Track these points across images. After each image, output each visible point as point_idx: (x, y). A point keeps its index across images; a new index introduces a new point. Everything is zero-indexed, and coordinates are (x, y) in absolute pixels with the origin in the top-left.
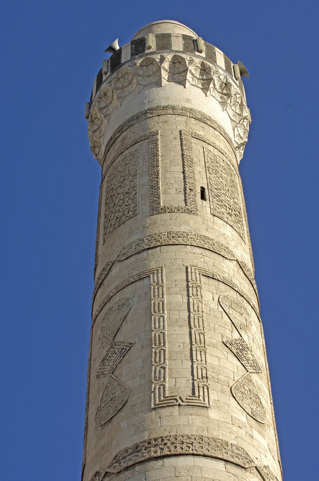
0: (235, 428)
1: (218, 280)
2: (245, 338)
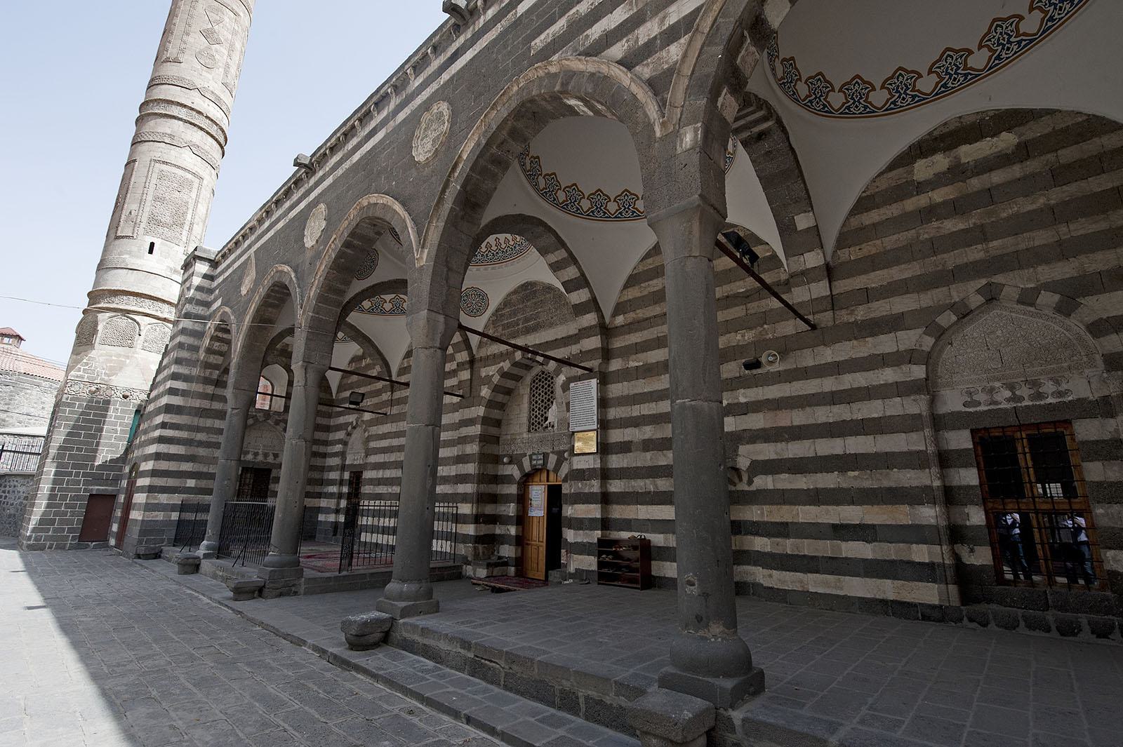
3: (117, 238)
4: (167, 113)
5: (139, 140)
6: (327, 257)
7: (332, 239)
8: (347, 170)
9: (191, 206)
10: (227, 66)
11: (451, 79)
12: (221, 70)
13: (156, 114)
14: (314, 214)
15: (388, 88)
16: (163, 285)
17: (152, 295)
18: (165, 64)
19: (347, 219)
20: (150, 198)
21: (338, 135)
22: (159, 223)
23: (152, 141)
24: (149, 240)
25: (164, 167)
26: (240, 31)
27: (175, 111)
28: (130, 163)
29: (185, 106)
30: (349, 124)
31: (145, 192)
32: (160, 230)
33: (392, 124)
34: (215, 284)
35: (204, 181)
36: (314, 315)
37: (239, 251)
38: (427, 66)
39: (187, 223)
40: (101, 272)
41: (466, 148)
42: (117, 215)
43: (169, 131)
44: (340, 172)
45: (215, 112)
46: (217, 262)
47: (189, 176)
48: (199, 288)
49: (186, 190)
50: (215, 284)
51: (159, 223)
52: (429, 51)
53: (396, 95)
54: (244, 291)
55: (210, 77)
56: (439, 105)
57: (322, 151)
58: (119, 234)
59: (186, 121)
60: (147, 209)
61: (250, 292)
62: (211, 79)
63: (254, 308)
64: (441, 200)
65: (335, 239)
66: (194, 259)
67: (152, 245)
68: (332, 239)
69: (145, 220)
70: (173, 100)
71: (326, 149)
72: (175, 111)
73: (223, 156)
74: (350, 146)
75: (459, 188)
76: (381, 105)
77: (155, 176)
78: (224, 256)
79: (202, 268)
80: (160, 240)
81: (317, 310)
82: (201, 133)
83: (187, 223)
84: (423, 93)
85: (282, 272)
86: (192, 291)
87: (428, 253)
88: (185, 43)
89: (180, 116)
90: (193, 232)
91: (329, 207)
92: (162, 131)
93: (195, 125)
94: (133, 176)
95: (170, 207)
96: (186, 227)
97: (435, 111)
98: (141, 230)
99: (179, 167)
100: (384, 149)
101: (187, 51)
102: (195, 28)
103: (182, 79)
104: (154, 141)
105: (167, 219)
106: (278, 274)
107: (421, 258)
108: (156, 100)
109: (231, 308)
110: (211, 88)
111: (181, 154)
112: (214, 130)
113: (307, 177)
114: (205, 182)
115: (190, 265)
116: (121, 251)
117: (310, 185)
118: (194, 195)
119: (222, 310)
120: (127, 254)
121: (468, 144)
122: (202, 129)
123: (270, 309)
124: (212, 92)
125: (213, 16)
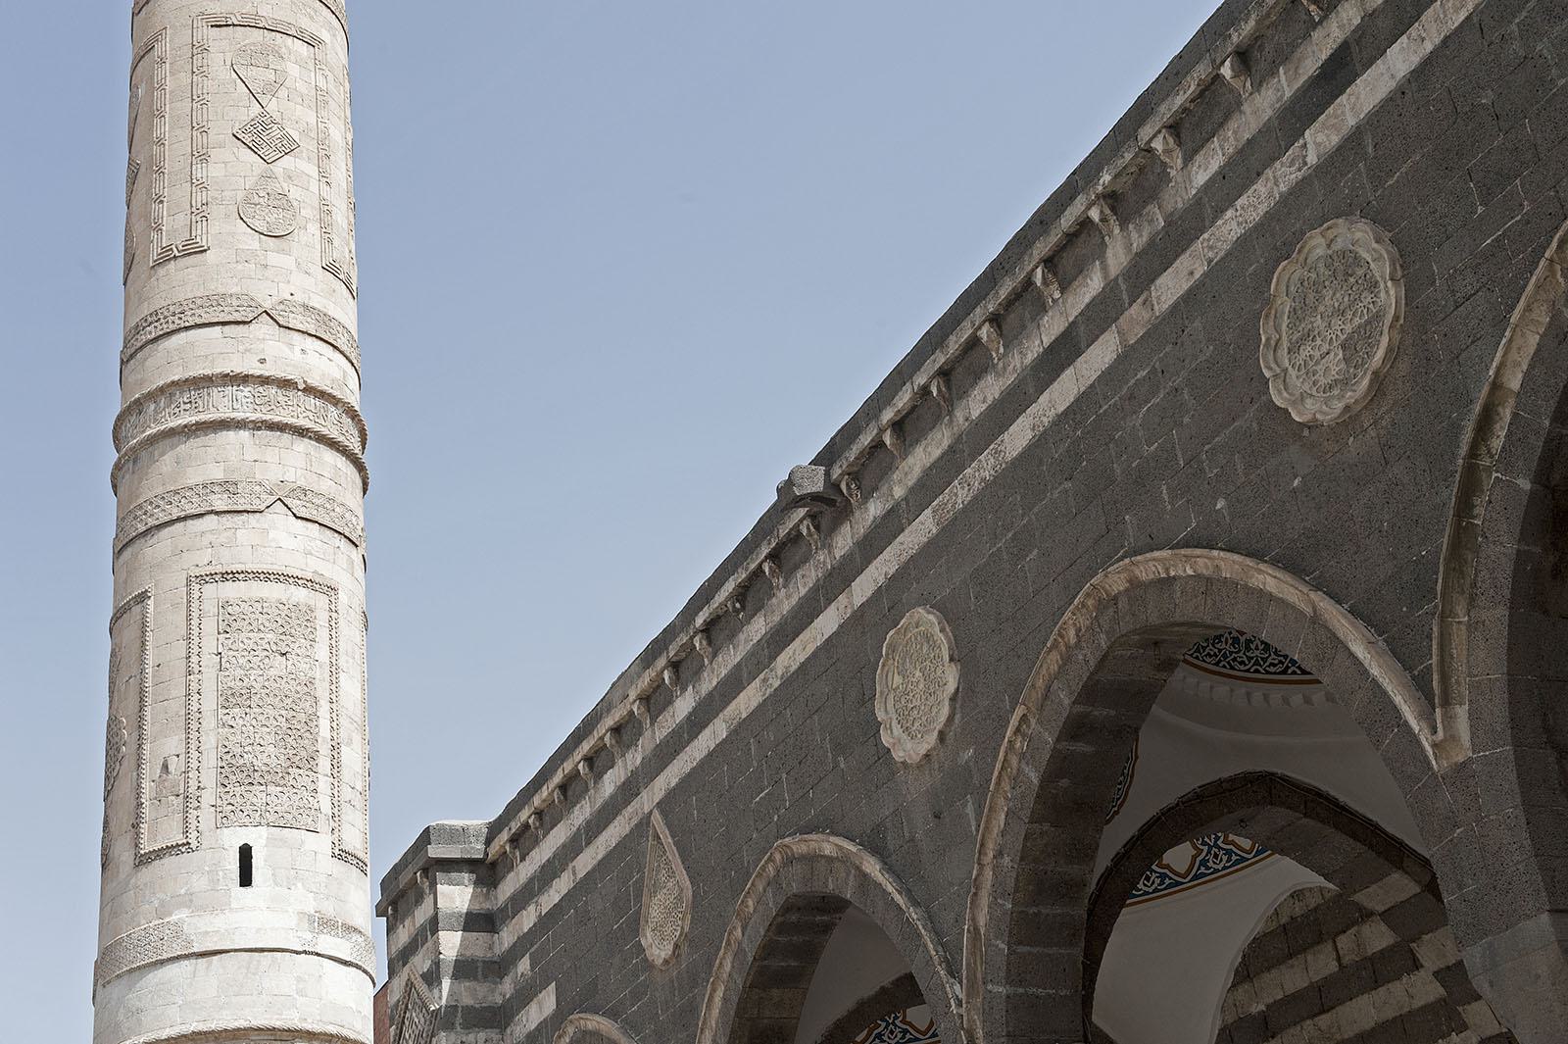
0: (240, 267)
1: (234, 25)
2: (272, 107)
3: (143, 860)
4: (203, 417)
5: (142, 528)
6: (1006, 786)
7: (1014, 722)
8: (989, 486)
9: (322, 690)
10: (325, 209)
11: (1353, 141)
12: (314, 228)
13: (172, 433)
14: (893, 648)
15: (1088, 208)
16: (299, 979)
17: (278, 1024)
18: (161, 271)
19: (1055, 645)
20: (209, 702)
21: (921, 379)
22: (251, 776)
23: (179, 519)
24: (233, 839)
25: (230, 590)
26: (331, 87)
27: (222, 404)
28: (128, 612)
29: (244, 379)
30: (955, 343)
31: (194, 686)
32: (258, 795)
33: (1137, 318)
34: (507, 937)
35: (341, 594)
36: (1011, 990)
37: (581, 814)
38: (1227, 117)
39: (324, 749)
40: (115, 990)
41: (1514, 355)
42: (124, 788)
43: (218, 474)
44: (959, 494)
45: (312, 359)
46: (494, 864)
47: (300, 595)
48: (464, 969)
49: (299, 646)
50: (507, 937)
51: (251, 776)
52: (1226, 71)
53: (1123, 224)
54: (658, 949)
55: (288, 262)
56: (1330, 234)
57: (866, 439)
58: (146, 847)
59: (258, 426)
60: (209, 741)
61: (685, 949)
62: (293, 267)
63: (725, 999)
64: (1463, 537)
65: (1024, 719)
66: (425, 871)
67: (246, 853)
68: (1014, 722)
69: (209, 778)
70: (208, 372)
71: (882, 431)
72: (222, 404)
73: (364, 493)
74: (976, 403)
75: (1525, 484)
76: (1067, 262)
77: (210, 626)
78: (524, 840)
79: (456, 896)
80: (263, 830)
81: (1016, 973)
82: (304, 445)
83: (324, 749)
84: (1239, 202)
85: (812, 859)
86: (446, 983)
87: (1473, 716)
88: (203, 187)
89: (239, 416)
90: (345, 771)
91: (949, 615)
92: (199, 480)
93: (280, 427)
94: (149, 646)
95: (272, 712)
96: (324, 764)
97: (1320, 251)
98: (206, 816)
99: (266, 576)
100: (1131, 397)
101: (214, 211)
102: (220, 131)
103: (217, 300)
104: (185, 518)
105: (269, 755)
106: (797, 869)
107: (1452, 737)
108: (162, 390)
109: (613, 1014)
110: (299, 298)
111: (266, 531)
112: (333, 424)
113: (817, 528)
114: (343, 597)
115: (412, 898)
116: (162, 903)
117: (838, 554)
118: (322, 653)
119: (571, 1030)
120: (181, 905)
121: (1518, 341)
122: (301, 432)
123: (775, 993)
124: (306, 307)
125: (258, 76)
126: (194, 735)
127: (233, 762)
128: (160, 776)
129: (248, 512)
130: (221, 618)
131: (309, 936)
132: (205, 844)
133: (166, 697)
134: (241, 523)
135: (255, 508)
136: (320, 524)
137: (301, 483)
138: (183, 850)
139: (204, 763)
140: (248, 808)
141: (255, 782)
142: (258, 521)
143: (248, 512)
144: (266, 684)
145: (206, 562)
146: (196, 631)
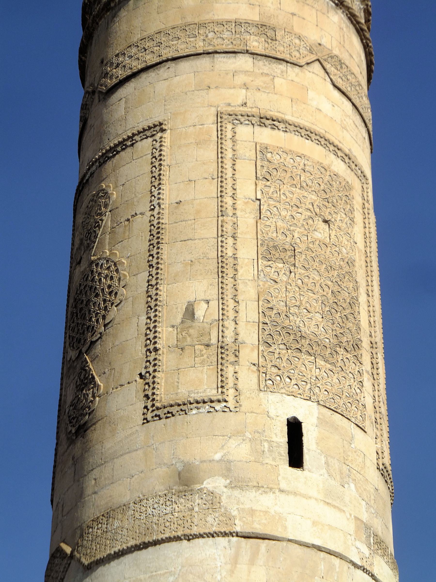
126: (229, 281)
127: (278, 320)
128: (182, 322)
129: (287, 62)
130: (259, 164)
131: (366, 551)
132: (245, 404)
133: (191, 236)
134: (279, 71)
135: (294, 60)
136: (353, 104)
137: (336, 52)
138: (217, 408)
139: (242, 315)
140: (295, 374)
141: (304, 350)
142: (297, 75)
143: (287, 62)
144: (311, 246)
145: (240, 102)
146: (229, 172)
